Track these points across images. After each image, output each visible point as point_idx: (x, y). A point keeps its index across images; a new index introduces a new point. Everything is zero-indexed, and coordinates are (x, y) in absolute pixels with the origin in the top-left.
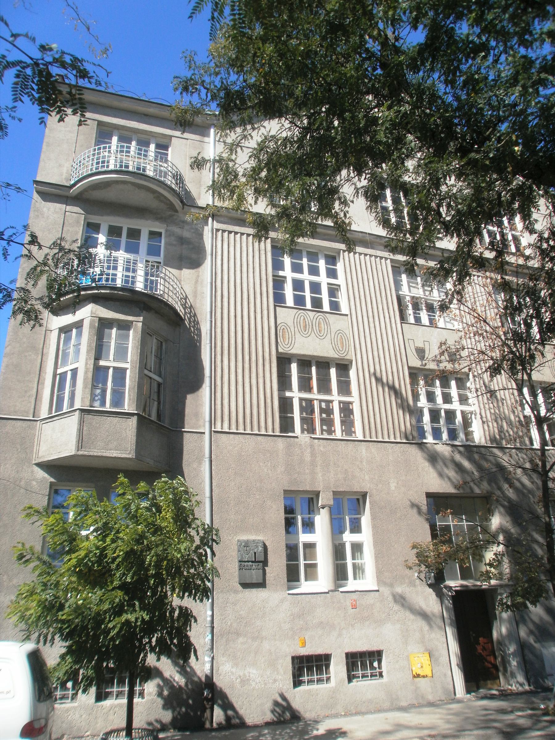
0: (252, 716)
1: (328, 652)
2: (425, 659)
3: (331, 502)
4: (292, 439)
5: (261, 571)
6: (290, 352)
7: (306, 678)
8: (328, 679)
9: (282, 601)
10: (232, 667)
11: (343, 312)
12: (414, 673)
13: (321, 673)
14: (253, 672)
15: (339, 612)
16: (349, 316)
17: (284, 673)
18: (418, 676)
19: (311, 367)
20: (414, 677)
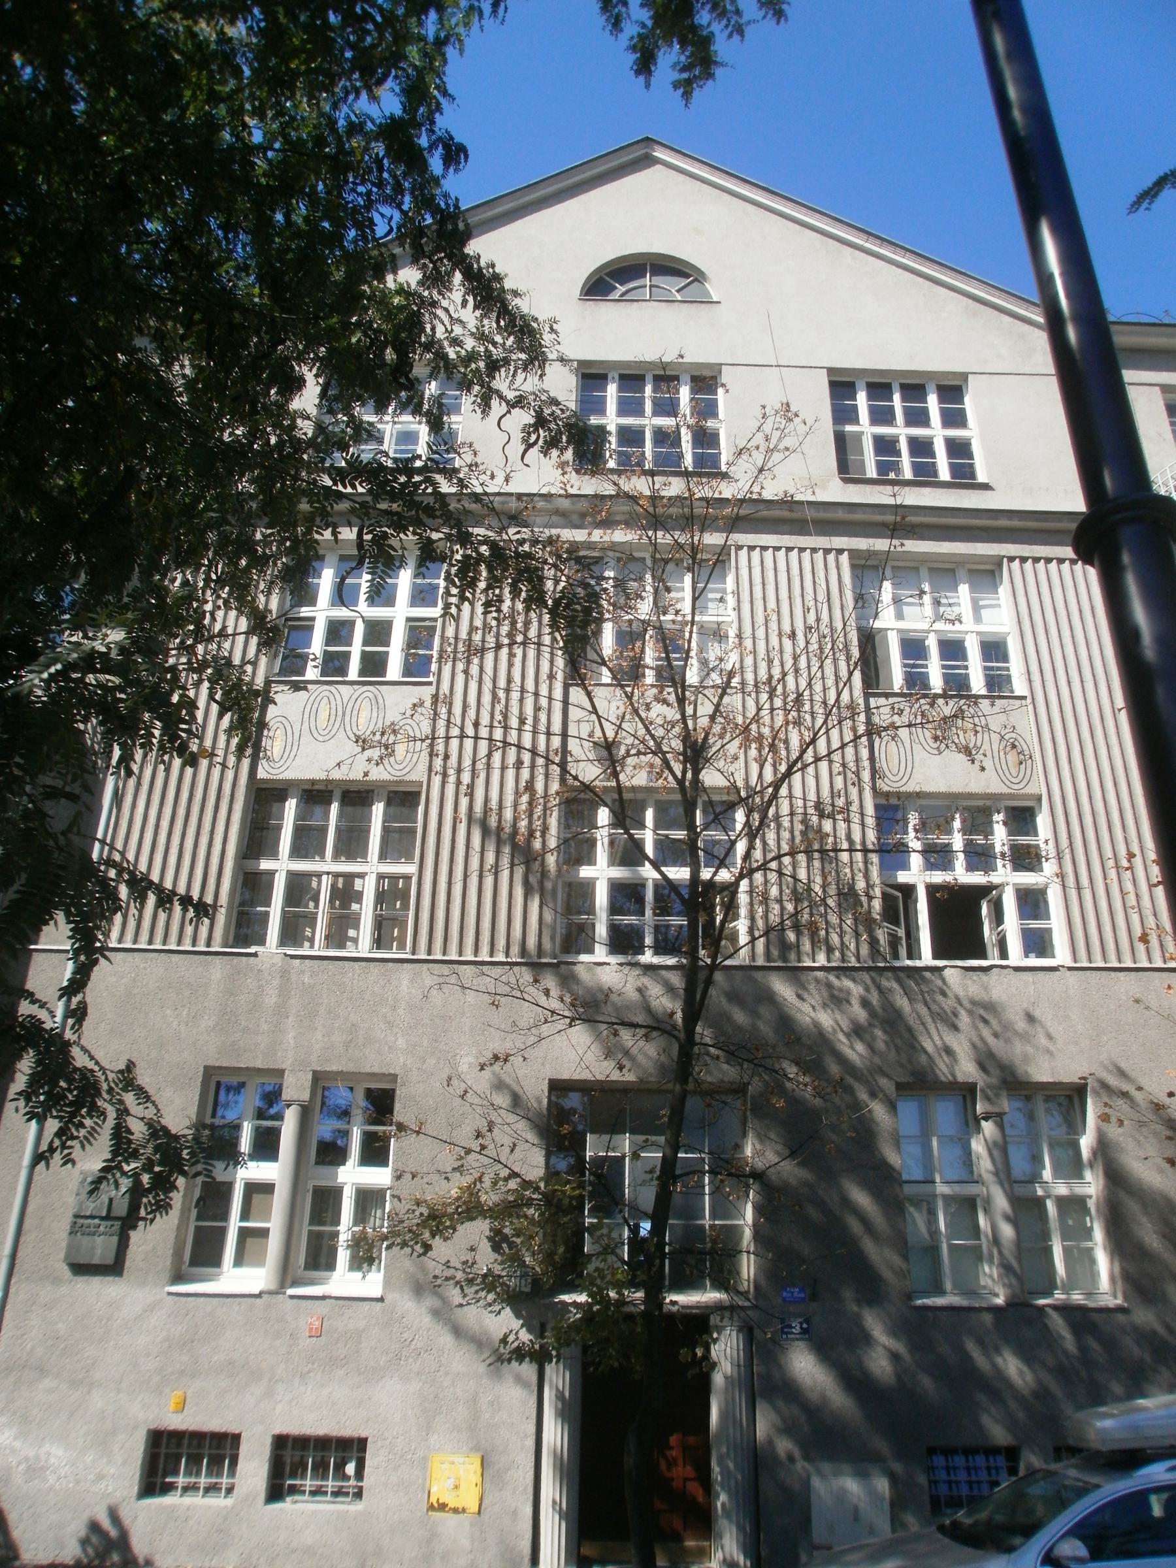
0: (33, 1545)
1: (233, 1428)
2: (468, 1470)
3: (306, 1096)
4: (244, 959)
5: (115, 1239)
6: (281, 777)
7: (181, 1480)
8: (230, 1490)
9: (151, 1308)
10: (15, 1438)
11: (1017, 693)
12: (433, 1500)
13: (219, 1474)
14: (56, 1454)
15: (278, 1342)
16: (1029, 700)
17: (124, 1463)
18: (442, 1507)
19: (643, 810)
20: (431, 1507)
